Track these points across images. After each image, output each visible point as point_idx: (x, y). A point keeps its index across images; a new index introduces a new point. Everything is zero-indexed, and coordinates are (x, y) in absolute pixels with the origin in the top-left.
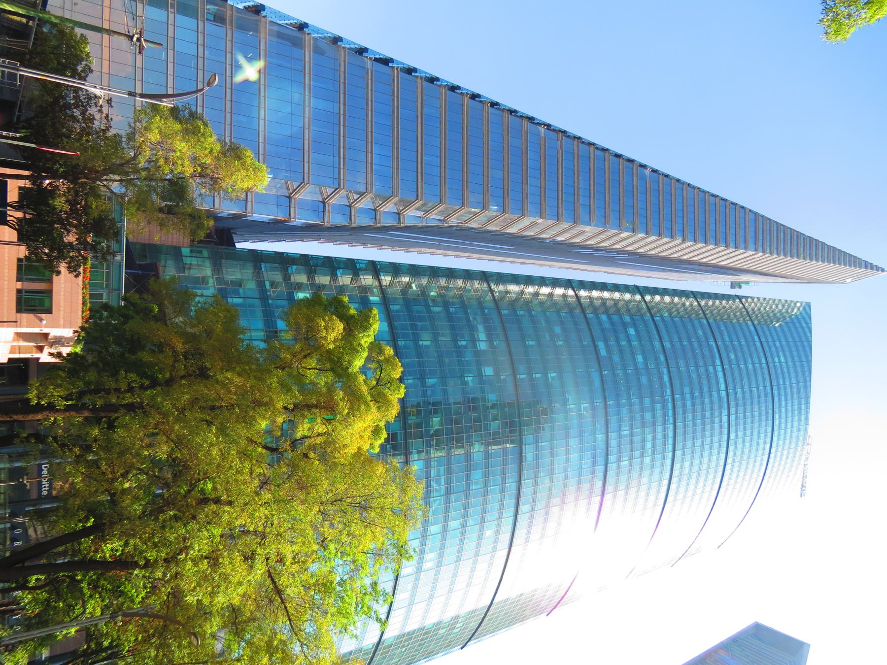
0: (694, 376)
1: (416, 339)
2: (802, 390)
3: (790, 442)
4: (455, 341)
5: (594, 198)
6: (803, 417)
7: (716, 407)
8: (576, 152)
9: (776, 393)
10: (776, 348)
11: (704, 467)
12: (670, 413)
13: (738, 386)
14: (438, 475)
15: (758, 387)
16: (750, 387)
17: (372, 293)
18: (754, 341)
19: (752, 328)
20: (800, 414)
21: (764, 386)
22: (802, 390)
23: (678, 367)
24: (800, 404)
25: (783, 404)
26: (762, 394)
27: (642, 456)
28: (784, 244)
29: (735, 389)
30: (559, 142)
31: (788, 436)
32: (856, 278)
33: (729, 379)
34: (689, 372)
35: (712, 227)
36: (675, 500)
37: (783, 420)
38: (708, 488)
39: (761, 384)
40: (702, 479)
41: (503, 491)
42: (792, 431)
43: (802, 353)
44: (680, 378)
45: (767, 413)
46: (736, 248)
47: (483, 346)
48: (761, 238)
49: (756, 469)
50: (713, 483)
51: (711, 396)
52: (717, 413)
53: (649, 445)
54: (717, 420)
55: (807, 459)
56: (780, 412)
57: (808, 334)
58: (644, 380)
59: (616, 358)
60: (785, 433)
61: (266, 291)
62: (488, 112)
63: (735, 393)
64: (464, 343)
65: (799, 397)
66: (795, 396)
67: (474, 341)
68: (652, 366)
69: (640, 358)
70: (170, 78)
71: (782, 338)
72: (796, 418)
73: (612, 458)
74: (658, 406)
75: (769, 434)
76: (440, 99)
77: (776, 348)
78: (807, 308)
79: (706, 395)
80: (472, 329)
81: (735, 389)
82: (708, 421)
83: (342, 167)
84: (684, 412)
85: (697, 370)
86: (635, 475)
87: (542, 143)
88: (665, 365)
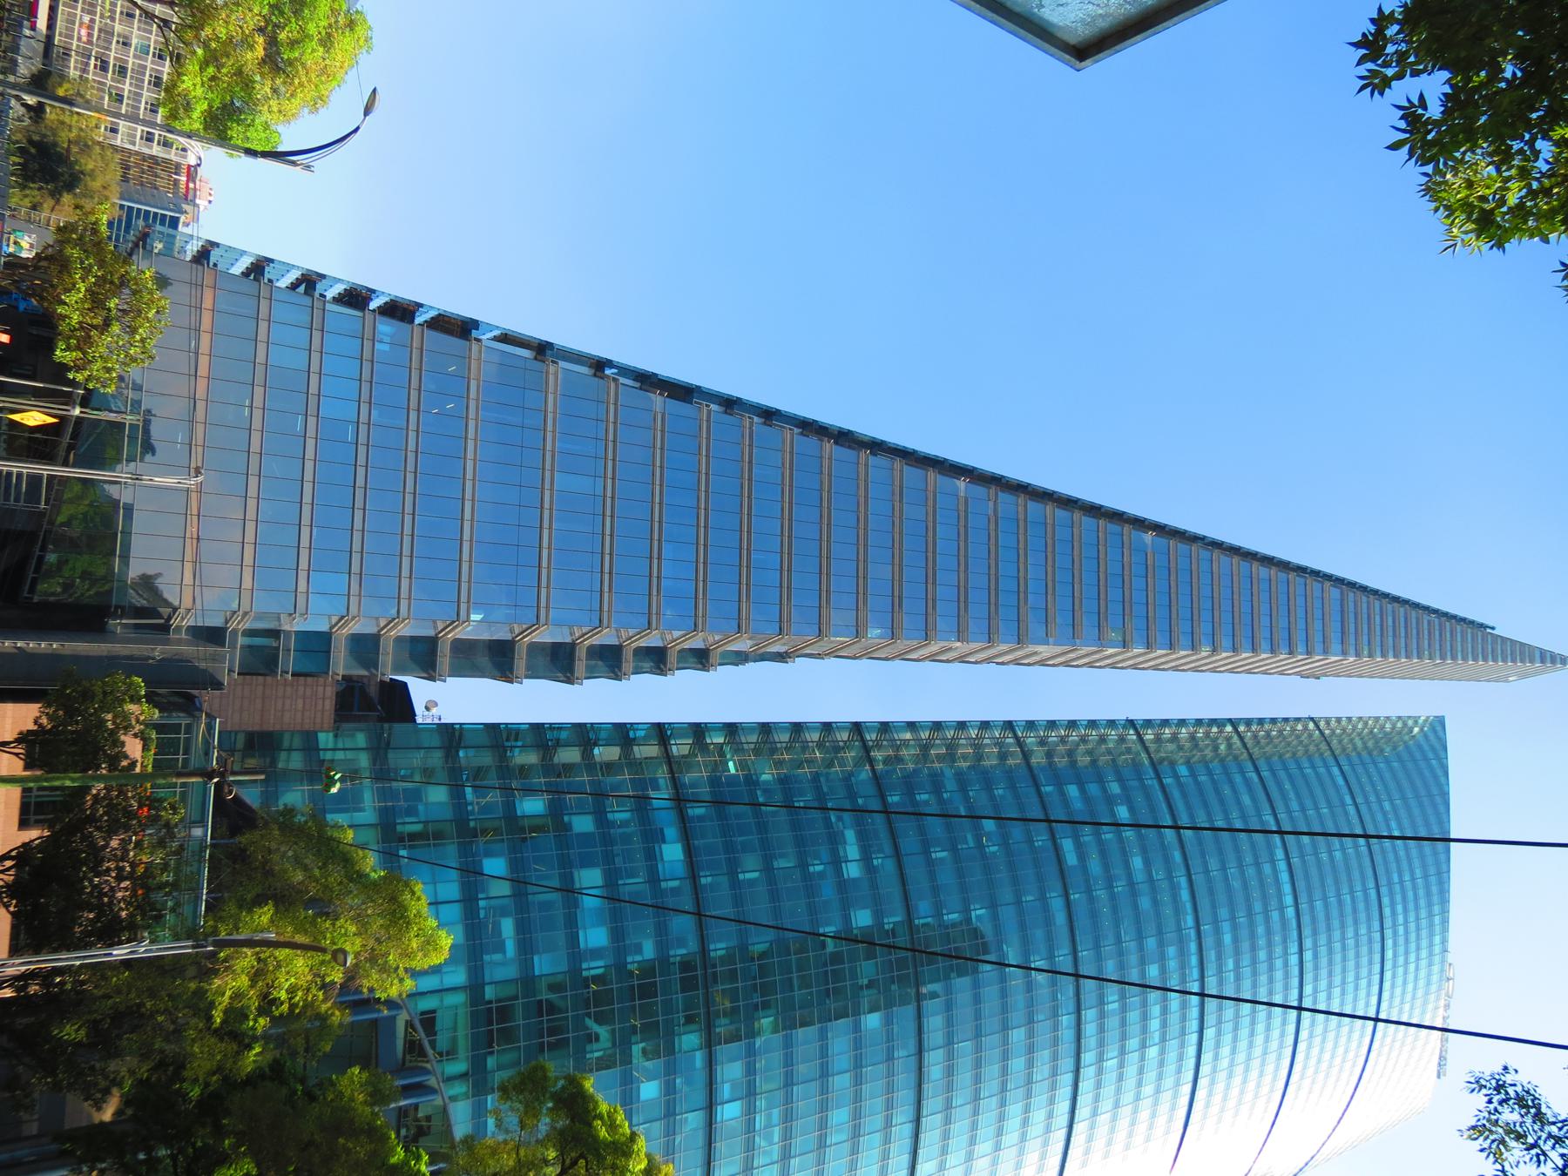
0: (1236, 884)
1: (733, 869)
2: (1434, 889)
3: (1415, 988)
4: (803, 865)
5: (1054, 594)
6: (1437, 939)
7: (1277, 938)
8: (1021, 516)
9: (1386, 901)
10: (1384, 813)
11: (1257, 1051)
12: (1194, 960)
13: (1317, 894)
14: (769, 1126)
15: (1352, 892)
16: (1338, 895)
17: (656, 788)
18: (1343, 805)
19: (1340, 781)
20: (1431, 935)
21: (1365, 890)
22: (1434, 889)
23: (1207, 871)
24: (1431, 915)
25: (1401, 919)
26: (1361, 906)
27: (1143, 1046)
28: (1394, 636)
29: (1311, 902)
30: (991, 504)
31: (1411, 977)
32: (1523, 676)
33: (1301, 885)
34: (1226, 879)
35: (1265, 621)
36: (1205, 1117)
37: (1401, 950)
38: (1265, 1090)
39: (1358, 887)
40: (1254, 1074)
41: (887, 1140)
42: (1417, 969)
43: (1430, 811)
44: (1211, 892)
45: (1370, 941)
46: (1308, 653)
47: (853, 871)
48: (1352, 626)
49: (1354, 1045)
50: (1274, 1079)
51: (1267, 920)
52: (1278, 950)
53: (1155, 1024)
54: (1279, 963)
55: (1447, 1007)
56: (1395, 933)
57: (1443, 779)
58: (1145, 903)
59: (1095, 866)
60: (1406, 973)
61: (467, 804)
62: (866, 465)
63: (1312, 908)
64: (819, 868)
65: (1430, 905)
66: (1422, 902)
67: (837, 862)
68: (1159, 874)
69: (1137, 862)
70: (309, 465)
71: (1396, 795)
72: (1424, 943)
73: (1088, 1057)
74: (1171, 951)
75: (1376, 978)
76: (783, 451)
77: (1384, 813)
78: (1439, 728)
79: (1259, 919)
80: (835, 840)
81: (1311, 902)
82: (1263, 967)
83: (606, 589)
84: (1219, 957)
85: (1242, 873)
86: (1130, 1082)
87: (962, 507)
88: (1183, 871)
